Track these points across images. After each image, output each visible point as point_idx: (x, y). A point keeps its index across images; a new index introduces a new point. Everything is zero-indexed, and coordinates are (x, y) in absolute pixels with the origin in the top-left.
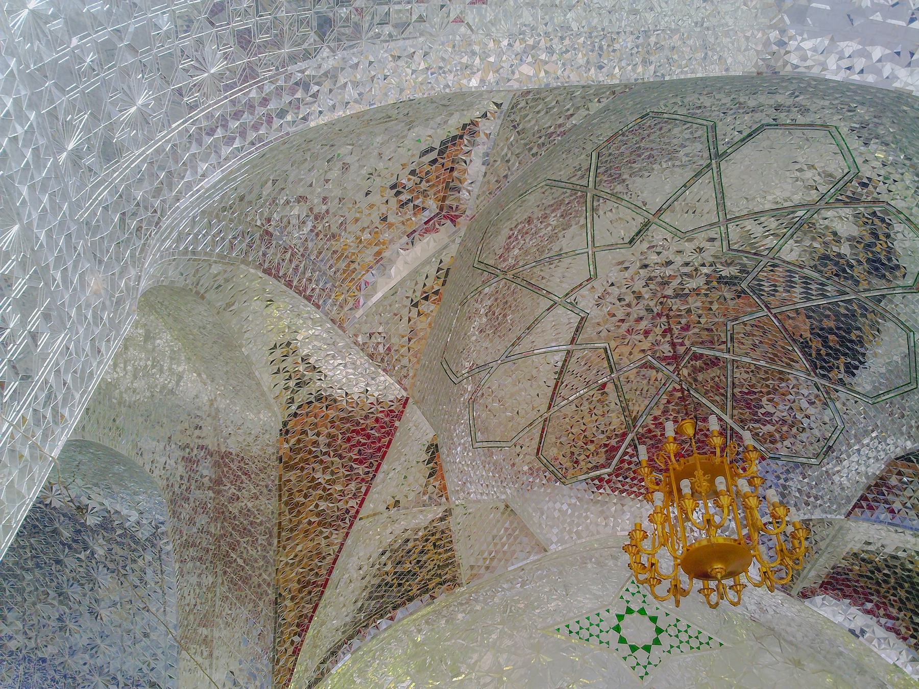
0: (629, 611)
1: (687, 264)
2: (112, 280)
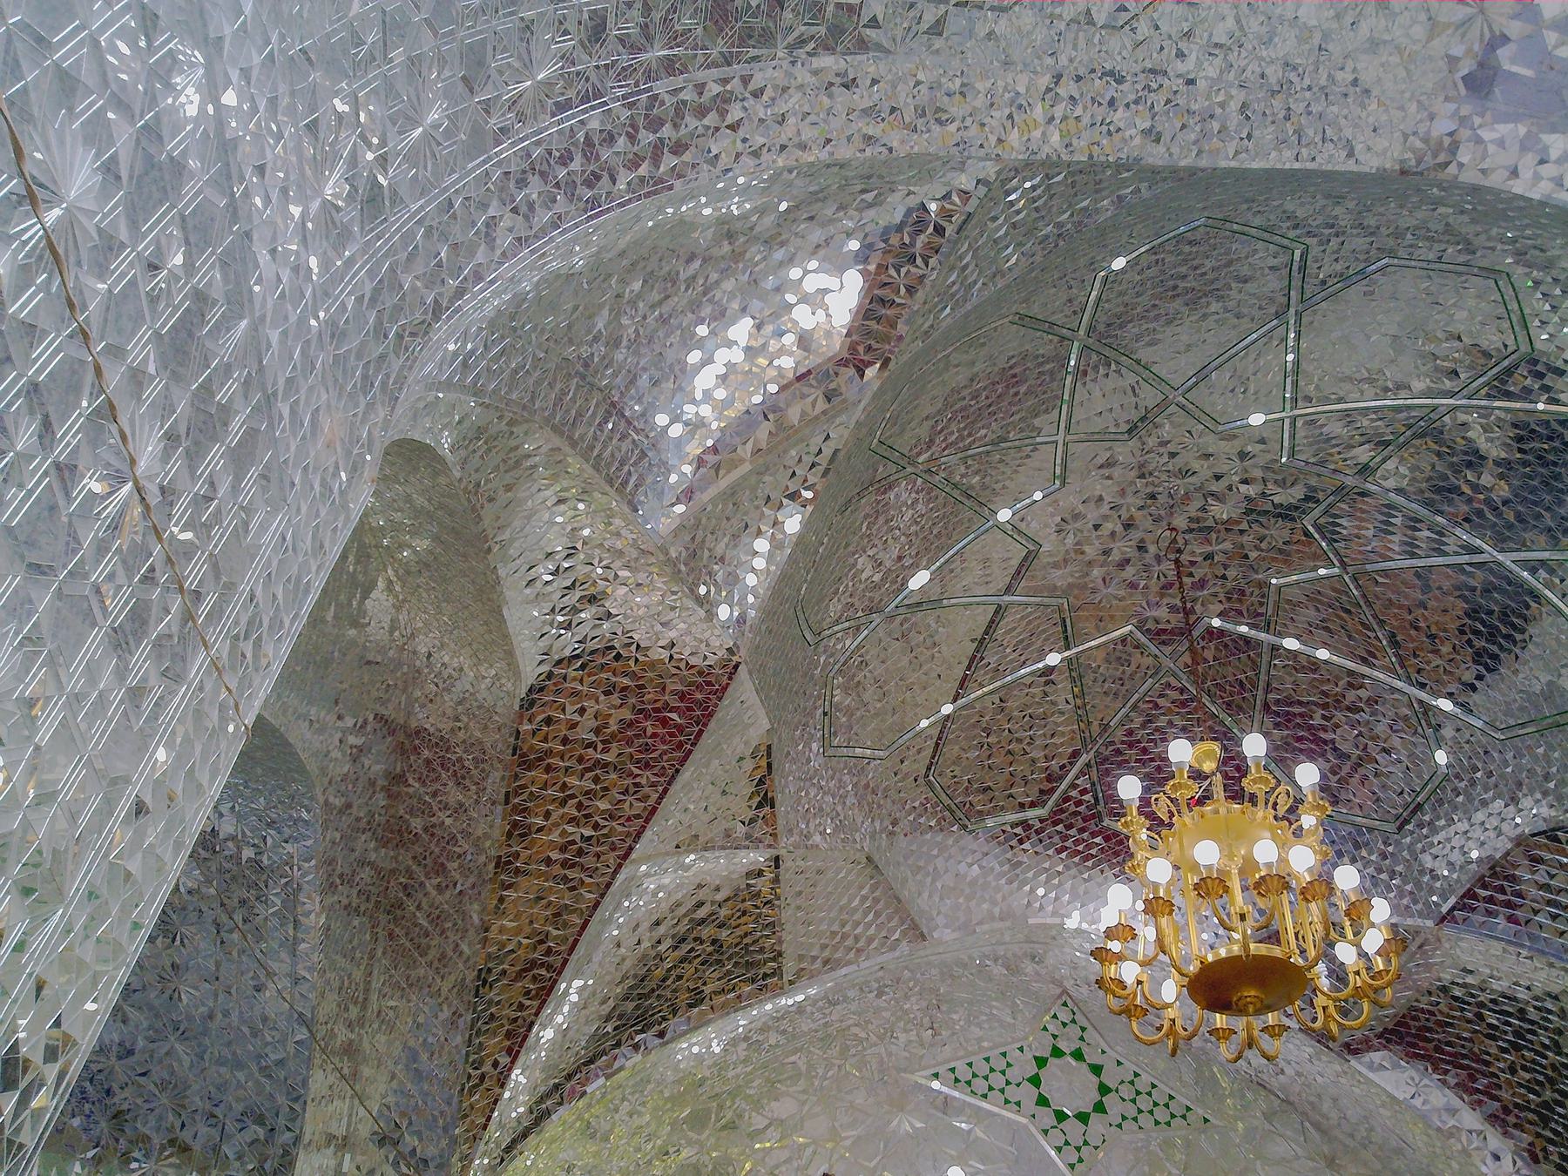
0: (1057, 1052)
1: (1218, 477)
2: (352, 424)
